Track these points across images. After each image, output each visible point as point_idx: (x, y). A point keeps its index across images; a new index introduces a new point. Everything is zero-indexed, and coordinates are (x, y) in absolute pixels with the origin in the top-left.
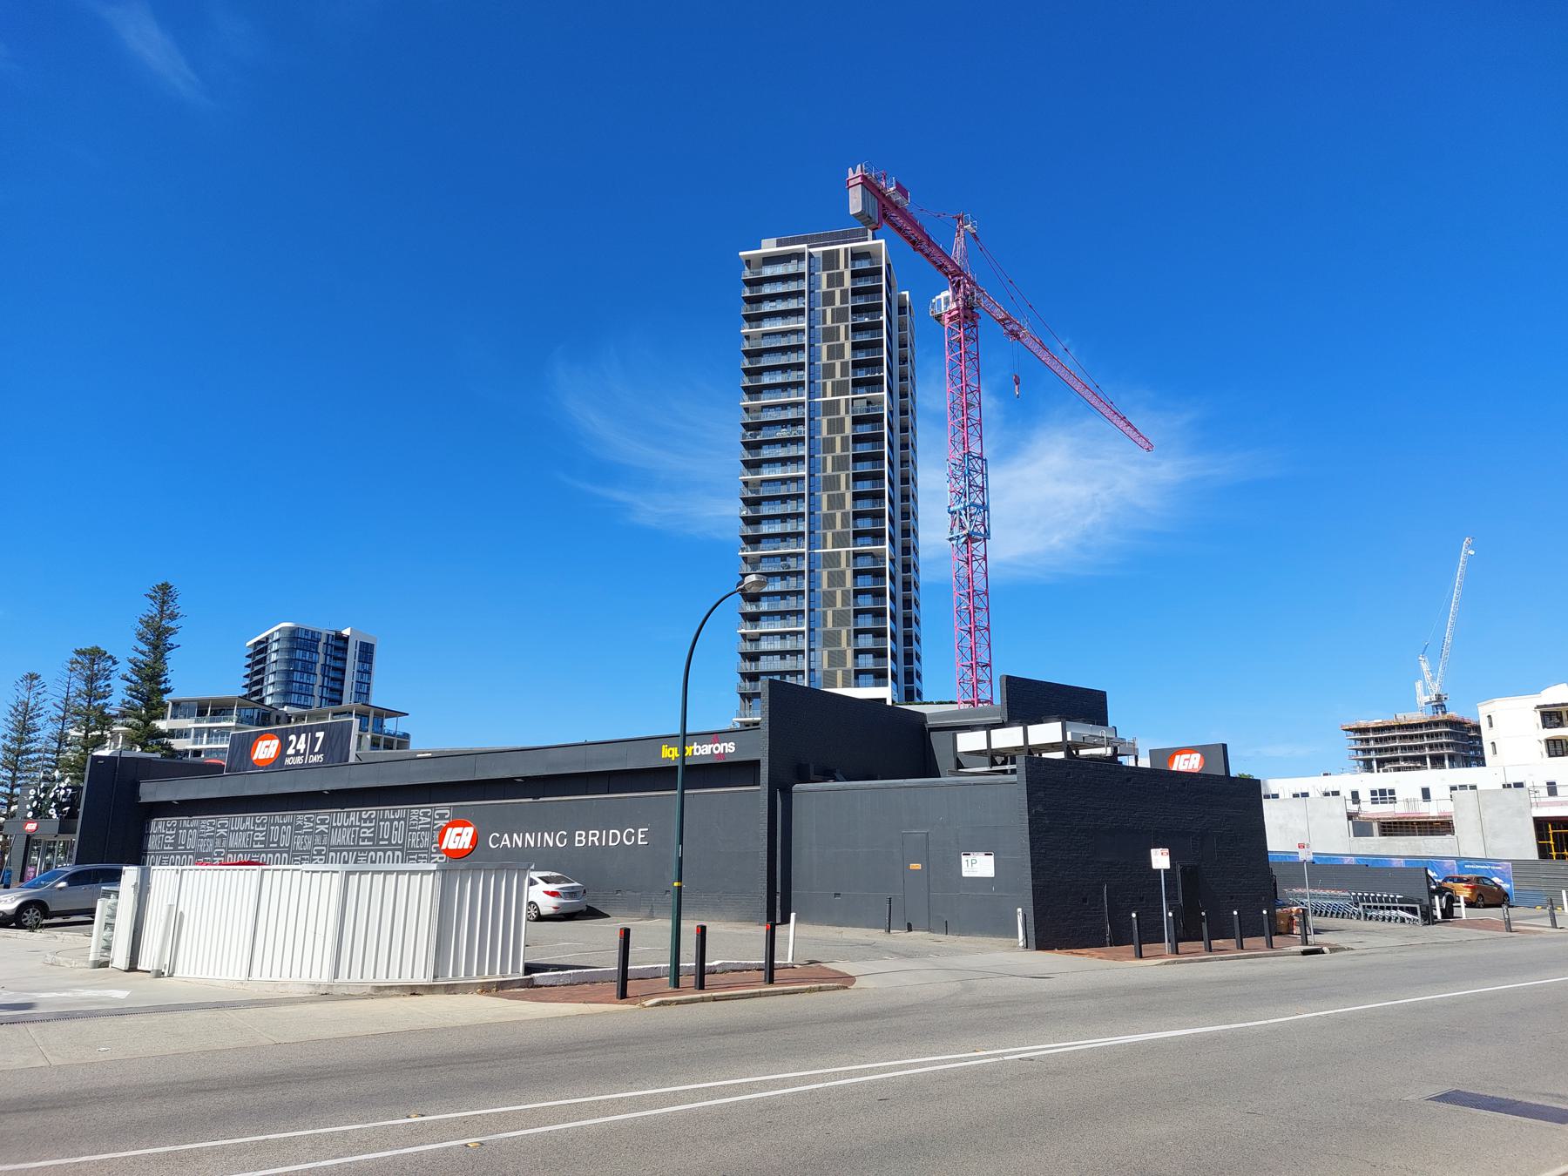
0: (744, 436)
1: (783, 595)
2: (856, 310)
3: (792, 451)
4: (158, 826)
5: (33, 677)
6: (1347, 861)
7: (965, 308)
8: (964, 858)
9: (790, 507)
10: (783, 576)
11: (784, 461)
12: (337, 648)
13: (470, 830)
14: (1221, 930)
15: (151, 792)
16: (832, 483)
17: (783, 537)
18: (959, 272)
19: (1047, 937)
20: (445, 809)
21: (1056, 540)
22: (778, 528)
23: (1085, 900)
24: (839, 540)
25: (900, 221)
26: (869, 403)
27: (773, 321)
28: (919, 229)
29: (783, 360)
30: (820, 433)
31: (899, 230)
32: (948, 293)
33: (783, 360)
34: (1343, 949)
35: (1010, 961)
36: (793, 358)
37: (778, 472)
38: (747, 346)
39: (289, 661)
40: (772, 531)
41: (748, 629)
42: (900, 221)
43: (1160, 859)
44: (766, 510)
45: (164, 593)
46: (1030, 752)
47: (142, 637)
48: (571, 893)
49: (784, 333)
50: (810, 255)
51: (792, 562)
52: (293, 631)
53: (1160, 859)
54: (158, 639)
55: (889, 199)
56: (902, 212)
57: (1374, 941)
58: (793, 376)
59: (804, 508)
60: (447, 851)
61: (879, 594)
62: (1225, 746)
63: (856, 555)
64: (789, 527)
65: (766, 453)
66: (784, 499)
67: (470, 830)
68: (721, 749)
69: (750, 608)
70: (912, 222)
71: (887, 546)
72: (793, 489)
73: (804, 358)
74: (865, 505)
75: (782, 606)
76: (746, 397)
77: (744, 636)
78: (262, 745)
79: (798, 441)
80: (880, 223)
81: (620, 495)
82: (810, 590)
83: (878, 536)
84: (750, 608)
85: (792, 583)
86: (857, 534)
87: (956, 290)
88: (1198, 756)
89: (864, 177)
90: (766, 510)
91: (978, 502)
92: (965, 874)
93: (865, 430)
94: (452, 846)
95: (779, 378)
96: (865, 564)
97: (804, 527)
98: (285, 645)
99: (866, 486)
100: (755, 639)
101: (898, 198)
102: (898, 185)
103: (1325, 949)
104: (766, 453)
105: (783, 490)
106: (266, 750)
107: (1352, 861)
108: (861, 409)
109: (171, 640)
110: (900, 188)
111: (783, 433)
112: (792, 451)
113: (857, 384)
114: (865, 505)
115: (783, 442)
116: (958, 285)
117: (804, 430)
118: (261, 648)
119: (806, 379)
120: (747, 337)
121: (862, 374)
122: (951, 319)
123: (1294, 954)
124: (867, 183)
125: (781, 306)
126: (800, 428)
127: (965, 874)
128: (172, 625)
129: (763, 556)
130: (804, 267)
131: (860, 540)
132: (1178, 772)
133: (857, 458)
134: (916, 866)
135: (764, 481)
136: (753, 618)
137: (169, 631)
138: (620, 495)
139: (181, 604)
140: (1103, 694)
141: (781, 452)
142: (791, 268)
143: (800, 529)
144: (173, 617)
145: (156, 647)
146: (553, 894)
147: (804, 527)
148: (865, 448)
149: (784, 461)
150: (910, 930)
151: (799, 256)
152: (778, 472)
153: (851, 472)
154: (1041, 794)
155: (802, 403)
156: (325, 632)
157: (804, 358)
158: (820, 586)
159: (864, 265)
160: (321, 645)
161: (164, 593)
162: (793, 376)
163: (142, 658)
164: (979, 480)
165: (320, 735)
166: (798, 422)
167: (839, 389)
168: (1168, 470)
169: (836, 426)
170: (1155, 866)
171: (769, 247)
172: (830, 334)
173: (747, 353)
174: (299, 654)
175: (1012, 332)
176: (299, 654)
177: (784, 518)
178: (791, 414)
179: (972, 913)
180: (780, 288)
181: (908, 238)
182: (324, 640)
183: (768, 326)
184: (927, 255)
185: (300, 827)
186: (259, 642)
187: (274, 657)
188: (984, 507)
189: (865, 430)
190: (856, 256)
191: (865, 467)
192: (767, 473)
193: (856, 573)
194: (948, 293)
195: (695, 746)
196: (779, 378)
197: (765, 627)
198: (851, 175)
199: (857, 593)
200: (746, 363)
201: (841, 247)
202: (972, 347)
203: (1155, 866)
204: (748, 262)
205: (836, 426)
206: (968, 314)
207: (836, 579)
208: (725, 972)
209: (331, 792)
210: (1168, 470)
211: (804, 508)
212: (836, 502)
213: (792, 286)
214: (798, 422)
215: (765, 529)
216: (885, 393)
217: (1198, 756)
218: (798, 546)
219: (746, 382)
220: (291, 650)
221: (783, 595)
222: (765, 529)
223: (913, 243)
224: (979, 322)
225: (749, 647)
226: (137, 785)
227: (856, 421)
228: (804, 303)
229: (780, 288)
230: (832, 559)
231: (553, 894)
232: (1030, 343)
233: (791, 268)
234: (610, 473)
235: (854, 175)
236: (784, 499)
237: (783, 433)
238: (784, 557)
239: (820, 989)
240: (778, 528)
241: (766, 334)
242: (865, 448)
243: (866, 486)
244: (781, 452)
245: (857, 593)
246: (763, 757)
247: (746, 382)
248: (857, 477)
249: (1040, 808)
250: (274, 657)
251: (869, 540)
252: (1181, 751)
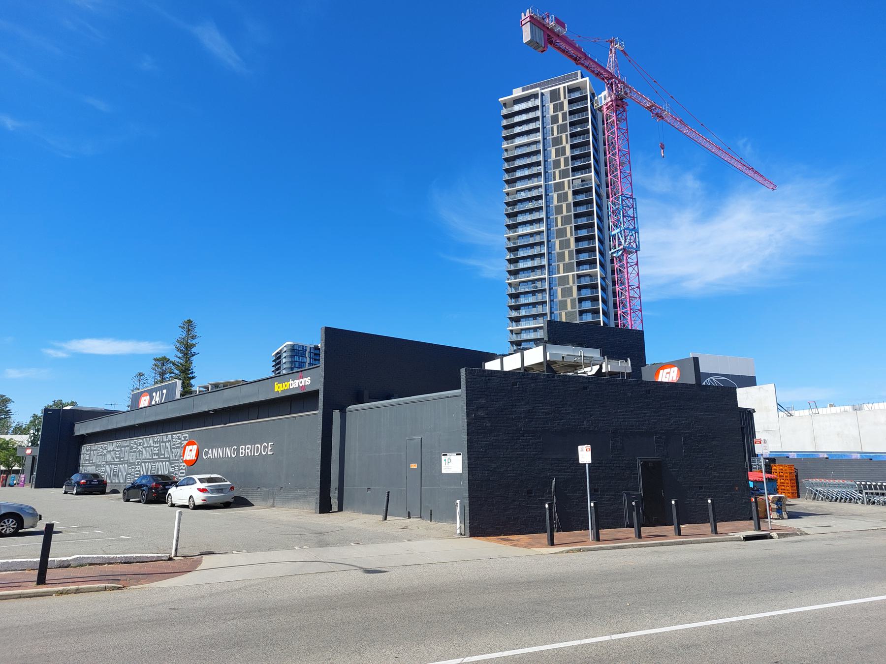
0: (506, 210)
1: (534, 305)
2: (572, 124)
3: (536, 216)
4: (85, 449)
5: (141, 375)
6: (854, 456)
7: (616, 100)
8: (443, 458)
9: (536, 250)
10: (533, 293)
11: (531, 223)
12: (316, 354)
13: (195, 447)
14: (690, 515)
15: (81, 429)
16: (561, 233)
17: (533, 269)
18: (611, 76)
19: (478, 527)
20: (186, 434)
21: (745, 266)
22: (529, 264)
23: (530, 492)
24: (568, 268)
25: (563, 45)
26: (583, 181)
27: (521, 138)
28: (578, 50)
29: (528, 161)
30: (552, 203)
31: (563, 51)
32: (606, 93)
33: (528, 161)
34: (806, 534)
35: (440, 549)
36: (534, 159)
37: (528, 230)
38: (506, 155)
39: (292, 362)
40: (526, 266)
41: (514, 327)
42: (563, 45)
43: (585, 455)
44: (521, 253)
45: (189, 325)
46: (525, 370)
47: (179, 350)
48: (219, 490)
49: (528, 145)
50: (542, 94)
51: (539, 284)
52: (293, 346)
53: (585, 455)
54: (187, 350)
55: (552, 30)
56: (564, 39)
57: (840, 525)
58: (534, 170)
59: (545, 250)
60: (186, 461)
61: (595, 299)
62: (696, 360)
63: (579, 277)
64: (536, 262)
65: (521, 219)
66: (532, 246)
67: (195, 447)
68: (303, 384)
69: (514, 314)
70: (572, 45)
71: (598, 269)
72: (537, 239)
73: (541, 158)
74: (584, 245)
75: (534, 311)
76: (506, 186)
77: (511, 331)
78: (143, 399)
79: (539, 209)
80: (546, 46)
81: (472, 262)
82: (551, 301)
83: (592, 263)
84: (514, 314)
85: (539, 297)
86: (579, 264)
87: (611, 89)
88: (676, 369)
89: (531, 17)
90: (521, 253)
91: (631, 227)
92: (443, 472)
93: (581, 198)
94: (188, 459)
95: (527, 172)
96: (585, 281)
97: (545, 262)
98: (289, 354)
99: (584, 233)
100: (518, 333)
101: (558, 29)
102: (556, 19)
103: (774, 534)
104: (521, 219)
105: (531, 240)
106: (144, 402)
107: (859, 456)
108: (578, 185)
109: (194, 350)
110: (558, 21)
111: (530, 205)
112: (536, 216)
113: (575, 170)
114: (584, 245)
115: (531, 211)
116: (612, 84)
117: (542, 203)
118: (278, 356)
119: (542, 171)
120: (506, 150)
121: (578, 164)
122: (608, 108)
123: (738, 540)
124: (533, 21)
125: (525, 128)
126: (540, 201)
127: (443, 472)
128: (194, 342)
129: (520, 282)
130: (538, 102)
131: (581, 267)
132: (661, 382)
133: (577, 216)
134: (414, 466)
135: (519, 236)
136: (517, 320)
137: (193, 345)
138: (472, 262)
139: (197, 331)
140: (641, 333)
141: (529, 217)
142: (530, 104)
143: (543, 263)
144: (193, 338)
145: (186, 354)
146: (203, 490)
147: (545, 262)
148: (582, 209)
149: (531, 223)
150: (410, 517)
151: (535, 96)
152: (528, 230)
153: (573, 225)
154: (483, 401)
155: (541, 186)
156: (309, 346)
157: (541, 158)
158: (557, 297)
159: (577, 95)
160: (307, 354)
161: (189, 325)
162: (534, 170)
163: (179, 360)
164: (630, 212)
165: (165, 391)
166: (539, 198)
167: (564, 174)
168: (820, 216)
169: (563, 197)
170: (581, 461)
171: (518, 93)
172: (557, 141)
173: (507, 160)
174: (296, 358)
175: (657, 114)
176: (296, 358)
177: (532, 257)
178: (534, 193)
179: (424, 503)
180: (524, 117)
181: (571, 56)
182: (308, 350)
183: (518, 141)
184: (587, 67)
185: (131, 448)
186: (278, 353)
187: (284, 360)
188: (636, 230)
189: (581, 198)
190: (571, 90)
191: (583, 221)
192: (521, 231)
193: (580, 288)
194: (606, 93)
195: (291, 382)
196: (527, 172)
197: (524, 325)
198: (523, 17)
199: (581, 300)
200: (506, 166)
201: (561, 86)
202: (623, 125)
203: (581, 461)
204: (505, 105)
205: (563, 197)
206: (619, 103)
207: (567, 292)
208: (82, 565)
209: (140, 425)
210: (820, 216)
211: (545, 250)
212: (565, 244)
213: (531, 115)
214: (539, 198)
215: (522, 265)
216: (593, 173)
217: (676, 369)
218: (542, 274)
219: (507, 177)
220: (292, 356)
221: (534, 305)
222: (522, 265)
223: (575, 59)
224: (627, 108)
225: (515, 338)
226: (74, 425)
227: (575, 193)
228: (539, 124)
229: (524, 117)
230: (564, 280)
231: (203, 490)
232: (669, 119)
233: (530, 104)
234: (468, 250)
235: (525, 17)
236: (532, 246)
237: (530, 205)
238: (533, 281)
239: (77, 591)
240: (529, 264)
241: (517, 147)
242: (582, 209)
243: (584, 233)
244: (529, 217)
245: (581, 300)
246: (320, 387)
247: (507, 177)
248: (577, 228)
249: (480, 413)
250: (284, 360)
251: (587, 266)
252: (664, 366)
